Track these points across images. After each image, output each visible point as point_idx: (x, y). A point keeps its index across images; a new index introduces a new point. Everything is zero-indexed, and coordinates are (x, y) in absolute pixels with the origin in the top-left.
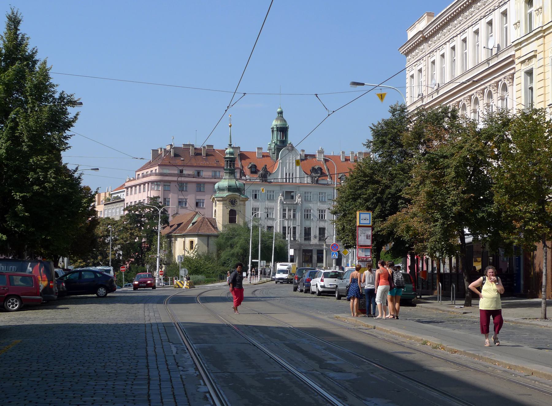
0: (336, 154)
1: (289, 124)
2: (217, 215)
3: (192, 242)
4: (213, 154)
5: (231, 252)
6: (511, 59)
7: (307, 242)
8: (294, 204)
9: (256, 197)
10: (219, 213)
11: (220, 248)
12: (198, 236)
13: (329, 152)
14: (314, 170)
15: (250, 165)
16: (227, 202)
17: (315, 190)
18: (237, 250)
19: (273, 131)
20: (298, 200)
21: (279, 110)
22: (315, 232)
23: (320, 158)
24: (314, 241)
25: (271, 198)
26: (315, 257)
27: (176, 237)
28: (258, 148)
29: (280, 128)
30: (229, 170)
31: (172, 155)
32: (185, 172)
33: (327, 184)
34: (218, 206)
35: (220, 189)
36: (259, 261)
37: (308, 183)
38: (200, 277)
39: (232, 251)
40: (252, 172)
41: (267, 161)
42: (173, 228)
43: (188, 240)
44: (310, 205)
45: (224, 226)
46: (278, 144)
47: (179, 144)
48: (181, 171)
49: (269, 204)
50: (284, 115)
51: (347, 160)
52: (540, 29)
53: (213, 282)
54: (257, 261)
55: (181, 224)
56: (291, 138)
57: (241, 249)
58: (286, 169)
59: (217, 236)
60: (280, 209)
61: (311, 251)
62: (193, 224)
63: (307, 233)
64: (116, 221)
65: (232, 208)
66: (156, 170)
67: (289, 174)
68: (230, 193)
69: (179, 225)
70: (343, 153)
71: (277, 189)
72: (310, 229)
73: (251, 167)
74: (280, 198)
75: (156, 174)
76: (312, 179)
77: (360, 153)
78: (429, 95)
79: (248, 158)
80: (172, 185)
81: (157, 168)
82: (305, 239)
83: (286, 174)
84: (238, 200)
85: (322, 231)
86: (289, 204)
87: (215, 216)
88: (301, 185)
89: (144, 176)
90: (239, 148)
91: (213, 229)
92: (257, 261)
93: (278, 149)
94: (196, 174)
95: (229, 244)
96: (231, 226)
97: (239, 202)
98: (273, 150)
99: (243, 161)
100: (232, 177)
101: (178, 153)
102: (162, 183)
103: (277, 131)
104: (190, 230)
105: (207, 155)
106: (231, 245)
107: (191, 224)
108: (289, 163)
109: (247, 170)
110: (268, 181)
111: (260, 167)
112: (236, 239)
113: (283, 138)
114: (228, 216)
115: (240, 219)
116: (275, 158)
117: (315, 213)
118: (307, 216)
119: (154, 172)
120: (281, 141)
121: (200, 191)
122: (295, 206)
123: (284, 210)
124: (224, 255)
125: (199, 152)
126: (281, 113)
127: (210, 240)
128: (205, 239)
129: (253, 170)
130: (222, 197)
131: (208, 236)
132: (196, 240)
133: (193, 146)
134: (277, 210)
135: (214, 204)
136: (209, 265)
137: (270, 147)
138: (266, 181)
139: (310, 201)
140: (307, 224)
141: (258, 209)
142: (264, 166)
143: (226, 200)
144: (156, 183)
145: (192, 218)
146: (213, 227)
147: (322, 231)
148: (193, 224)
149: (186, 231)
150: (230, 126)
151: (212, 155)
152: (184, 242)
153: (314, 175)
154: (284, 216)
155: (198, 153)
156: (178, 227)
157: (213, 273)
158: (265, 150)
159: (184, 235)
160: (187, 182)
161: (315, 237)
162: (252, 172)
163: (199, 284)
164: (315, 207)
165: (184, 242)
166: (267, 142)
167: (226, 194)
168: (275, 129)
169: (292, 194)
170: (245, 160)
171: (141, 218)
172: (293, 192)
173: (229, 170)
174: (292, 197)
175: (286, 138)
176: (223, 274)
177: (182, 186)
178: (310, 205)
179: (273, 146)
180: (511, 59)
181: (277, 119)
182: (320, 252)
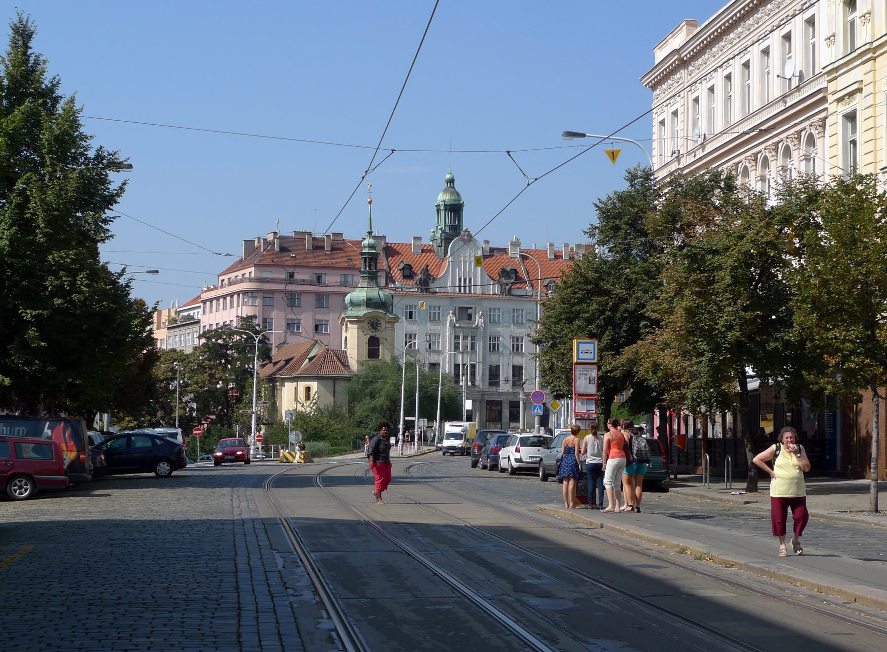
0: (539, 247)
1: (464, 199)
2: (348, 345)
3: (308, 389)
4: (342, 247)
5: (372, 405)
6: (821, 95)
7: (493, 389)
8: (472, 328)
9: (411, 317)
10: (352, 342)
11: (354, 398)
12: (318, 378)
13: (528, 244)
14: (504, 273)
15: (402, 265)
16: (366, 324)
17: (507, 306)
18: (381, 401)
19: (438, 211)
20: (479, 321)
21: (448, 177)
22: (506, 373)
23: (514, 253)
24: (505, 387)
25: (435, 318)
26: (506, 413)
27: (283, 381)
28: (415, 238)
29: (451, 205)
30: (369, 272)
31: (277, 248)
32: (297, 277)
33: (526, 296)
34: (350, 330)
35: (354, 304)
36: (416, 419)
37: (494, 294)
38: (321, 445)
39: (373, 402)
40: (405, 277)
41: (428, 259)
42: (278, 366)
43: (302, 385)
44: (499, 329)
45: (360, 363)
46: (447, 231)
47: (288, 231)
48: (292, 275)
49: (431, 328)
50: (457, 185)
51: (557, 256)
52: (867, 47)
53: (342, 452)
54: (413, 419)
55: (291, 359)
56: (468, 222)
57: (388, 399)
58: (460, 271)
59: (348, 379)
60: (451, 335)
61: (500, 403)
62: (310, 359)
63: (494, 374)
64: (187, 355)
65: (373, 334)
66: (250, 273)
67: (465, 280)
68: (370, 310)
69: (287, 361)
70: (551, 245)
71: (445, 303)
72: (498, 367)
73: (403, 269)
74: (450, 317)
75: (251, 280)
76: (501, 288)
77: (578, 246)
78: (689, 153)
79: (399, 254)
80: (277, 296)
81: (252, 269)
82: (491, 384)
83: (460, 279)
84: (382, 322)
85: (517, 371)
86: (464, 328)
87: (346, 347)
88: (484, 297)
89: (231, 283)
90: (385, 237)
91: (342, 367)
92: (413, 419)
93: (447, 239)
94: (315, 279)
95: (368, 391)
96: (372, 362)
97: (383, 325)
98: (439, 241)
99: (390, 259)
100: (373, 284)
101: (286, 246)
102: (261, 295)
103: (446, 210)
104: (306, 370)
105: (333, 249)
106: (371, 393)
107: (307, 360)
108: (465, 262)
109: (397, 274)
110: (431, 290)
111: (418, 269)
112: (379, 384)
113: (454, 222)
114: (366, 347)
115: (386, 352)
116: (442, 254)
117: (506, 343)
118: (494, 348)
119: (247, 275)
120: (451, 227)
121: (322, 307)
122: (474, 330)
123: (457, 337)
124: (360, 409)
125: (319, 244)
126: (451, 181)
127: (337, 385)
128: (330, 383)
129: (407, 272)
130: (356, 317)
131: (335, 379)
132: (314, 385)
133: (310, 234)
134: (444, 336)
135: (344, 327)
136: (336, 426)
137: (434, 236)
138: (427, 291)
139: (499, 323)
140: (493, 359)
141: (415, 335)
142: (424, 267)
143: (362, 322)
144: (250, 295)
145: (309, 351)
146: (343, 364)
147: (517, 371)
148: (310, 359)
149: (299, 371)
150: (370, 203)
151: (341, 249)
152: (296, 389)
153: (504, 280)
154: (457, 347)
155: (317, 245)
156: (286, 365)
157: (342, 438)
158: (426, 241)
159: (295, 378)
160: (300, 293)
161: (507, 381)
162: (405, 277)
163: (320, 457)
164: (506, 333)
165: (296, 389)
166: (430, 228)
167: (362, 311)
168: (442, 208)
169: (469, 311)
170: (393, 256)
171: (227, 350)
172: (471, 308)
173: (369, 272)
174: (470, 317)
175: (459, 222)
176: (358, 441)
177: (292, 299)
178: (499, 329)
179: (438, 235)
180: (821, 95)
181: (445, 191)
182: (514, 405)
